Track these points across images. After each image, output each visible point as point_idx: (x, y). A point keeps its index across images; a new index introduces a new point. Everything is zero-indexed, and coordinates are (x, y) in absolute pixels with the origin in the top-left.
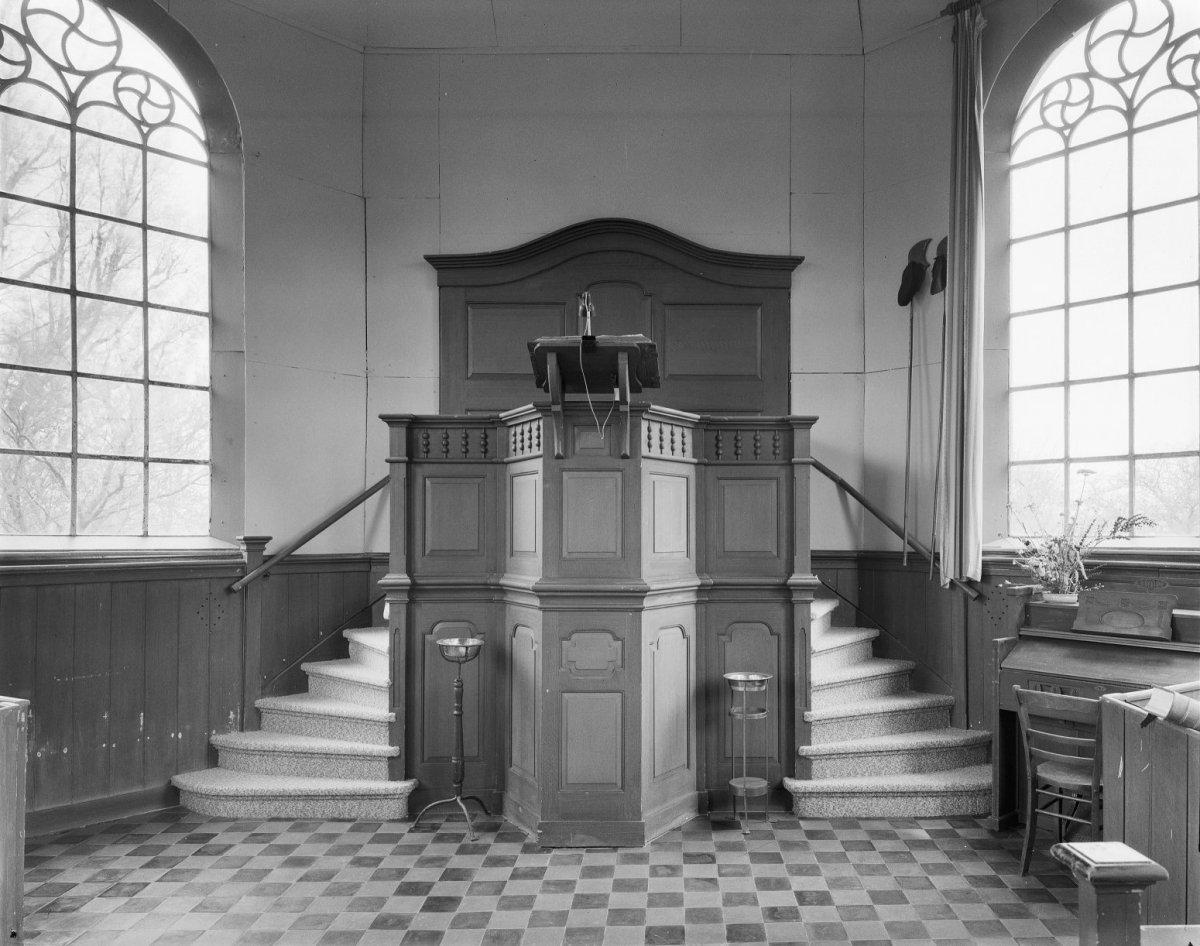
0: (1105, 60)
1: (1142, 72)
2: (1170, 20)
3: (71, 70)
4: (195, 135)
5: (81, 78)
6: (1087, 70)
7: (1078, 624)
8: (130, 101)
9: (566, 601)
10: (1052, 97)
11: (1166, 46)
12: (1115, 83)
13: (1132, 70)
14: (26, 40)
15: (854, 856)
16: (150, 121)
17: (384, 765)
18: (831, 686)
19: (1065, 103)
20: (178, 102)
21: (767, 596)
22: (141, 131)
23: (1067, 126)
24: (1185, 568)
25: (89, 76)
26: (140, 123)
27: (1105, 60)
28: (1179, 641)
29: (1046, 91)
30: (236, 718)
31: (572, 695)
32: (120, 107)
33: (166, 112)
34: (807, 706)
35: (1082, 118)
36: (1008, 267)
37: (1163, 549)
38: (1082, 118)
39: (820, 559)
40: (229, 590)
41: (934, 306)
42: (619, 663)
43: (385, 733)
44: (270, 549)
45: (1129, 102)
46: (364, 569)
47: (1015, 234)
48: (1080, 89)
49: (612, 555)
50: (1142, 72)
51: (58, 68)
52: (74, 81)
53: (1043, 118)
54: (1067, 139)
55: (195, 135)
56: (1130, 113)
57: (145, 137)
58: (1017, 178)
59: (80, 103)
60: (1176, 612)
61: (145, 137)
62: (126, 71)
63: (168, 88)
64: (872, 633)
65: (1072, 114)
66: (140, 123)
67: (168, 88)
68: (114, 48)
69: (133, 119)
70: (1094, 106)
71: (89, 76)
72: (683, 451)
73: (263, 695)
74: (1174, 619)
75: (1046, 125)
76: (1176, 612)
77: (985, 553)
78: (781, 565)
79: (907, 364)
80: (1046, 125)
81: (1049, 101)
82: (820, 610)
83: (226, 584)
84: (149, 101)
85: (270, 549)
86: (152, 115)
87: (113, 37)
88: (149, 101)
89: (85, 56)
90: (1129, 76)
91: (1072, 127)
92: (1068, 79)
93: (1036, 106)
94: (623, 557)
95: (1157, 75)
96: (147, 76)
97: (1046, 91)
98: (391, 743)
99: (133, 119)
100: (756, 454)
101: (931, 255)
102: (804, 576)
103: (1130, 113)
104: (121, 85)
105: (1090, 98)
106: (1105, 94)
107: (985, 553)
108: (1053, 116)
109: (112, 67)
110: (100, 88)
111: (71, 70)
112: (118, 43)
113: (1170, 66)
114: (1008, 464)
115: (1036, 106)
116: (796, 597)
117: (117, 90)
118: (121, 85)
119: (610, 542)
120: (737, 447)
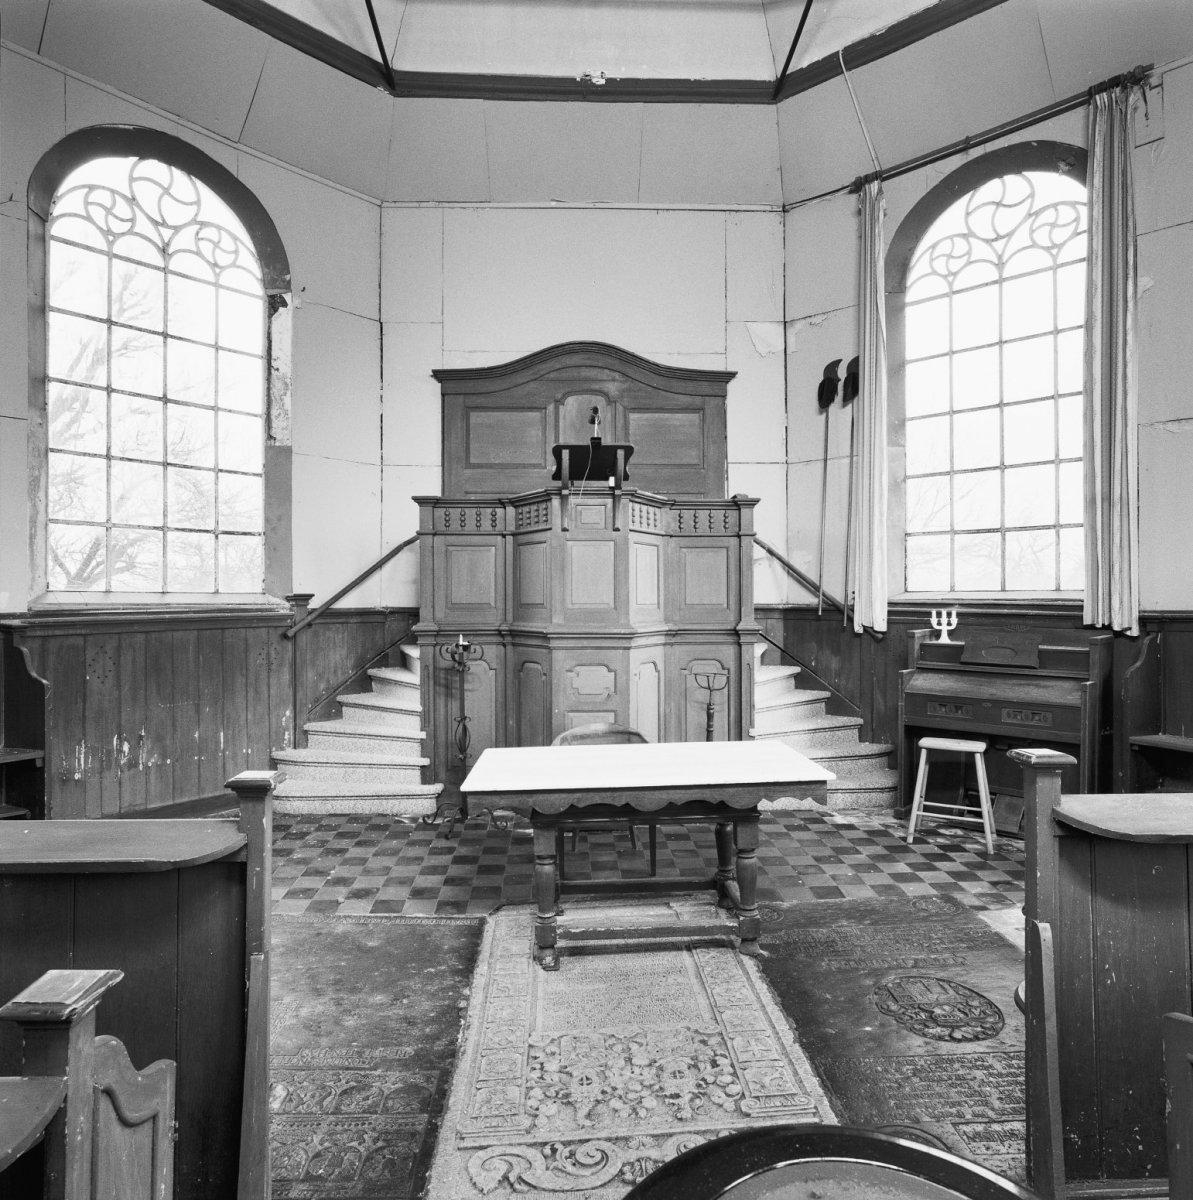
0: (981, 224)
1: (1009, 235)
2: (1032, 195)
3: (164, 224)
4: (254, 275)
5: (172, 231)
6: (966, 232)
7: (964, 658)
8: (206, 248)
9: (570, 641)
10: (938, 251)
11: (1030, 215)
12: (988, 241)
13: (1002, 232)
14: (132, 200)
15: (796, 835)
16: (115, 231)
17: (417, 773)
18: (769, 709)
19: (950, 256)
20: (242, 249)
21: (721, 639)
22: (214, 272)
23: (1055, 246)
24: (1046, 616)
25: (177, 229)
26: (107, 233)
27: (981, 224)
28: (1045, 668)
29: (934, 247)
30: (289, 739)
31: (576, 714)
32: (88, 218)
33: (129, 224)
34: (752, 725)
35: (962, 268)
36: (903, 385)
37: (1037, 600)
38: (962, 268)
39: (763, 611)
40: (285, 636)
41: (840, 413)
42: (613, 689)
43: (417, 747)
44: (314, 604)
45: (1000, 257)
46: (379, 620)
47: (909, 355)
48: (961, 246)
49: (606, 606)
50: (1009, 235)
51: (156, 223)
52: (167, 233)
53: (932, 267)
54: (1055, 257)
55: (254, 275)
56: (1000, 265)
57: (217, 275)
58: (909, 311)
59: (170, 251)
60: (1040, 647)
61: (217, 275)
62: (203, 224)
63: (235, 238)
64: (797, 669)
65: (955, 265)
66: (107, 233)
67: (235, 238)
68: (195, 207)
69: (100, 229)
70: (972, 259)
71: (177, 229)
72: (641, 523)
73: (309, 720)
74: (1041, 652)
75: (934, 272)
76: (1040, 647)
77: (890, 604)
78: (732, 617)
79: (822, 457)
80: (934, 272)
81: (936, 254)
82: (760, 648)
83: (280, 631)
84: (220, 248)
85: (314, 604)
86: (223, 259)
87: (193, 198)
88: (220, 248)
89: (175, 214)
90: (998, 238)
91: (955, 274)
92: (951, 237)
93: (927, 256)
94: (615, 608)
95: (1021, 238)
96: (219, 228)
97: (934, 247)
98: (423, 755)
99: (100, 229)
100: (710, 528)
101: (842, 373)
102: (749, 622)
103: (1000, 265)
104: (200, 236)
105: (969, 253)
106: (981, 250)
107: (890, 604)
108: (940, 266)
109: (194, 221)
110: (184, 239)
111: (164, 224)
112: (198, 203)
113: (1032, 231)
114: (48, 450)
115: (927, 256)
116: (743, 639)
117: (87, 203)
118: (200, 236)
119: (608, 598)
120: (726, 523)
